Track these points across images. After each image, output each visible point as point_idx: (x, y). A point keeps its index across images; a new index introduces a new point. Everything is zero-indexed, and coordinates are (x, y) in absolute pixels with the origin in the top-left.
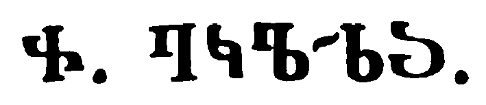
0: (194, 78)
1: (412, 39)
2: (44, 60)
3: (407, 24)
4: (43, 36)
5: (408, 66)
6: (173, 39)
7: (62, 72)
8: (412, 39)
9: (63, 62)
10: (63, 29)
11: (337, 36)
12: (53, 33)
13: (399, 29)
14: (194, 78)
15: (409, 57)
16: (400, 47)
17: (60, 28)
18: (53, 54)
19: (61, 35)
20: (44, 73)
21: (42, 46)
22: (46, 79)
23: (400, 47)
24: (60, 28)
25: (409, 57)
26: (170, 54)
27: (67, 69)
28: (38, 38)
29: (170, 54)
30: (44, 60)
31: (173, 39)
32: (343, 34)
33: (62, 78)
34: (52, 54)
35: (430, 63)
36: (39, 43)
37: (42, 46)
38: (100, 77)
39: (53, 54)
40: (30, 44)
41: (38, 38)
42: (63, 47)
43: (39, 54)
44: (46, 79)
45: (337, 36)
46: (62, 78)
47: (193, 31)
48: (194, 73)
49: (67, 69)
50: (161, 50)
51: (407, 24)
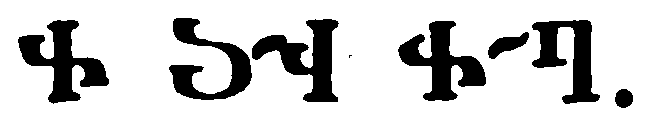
0: (335, 99)
1: (204, 43)
2: (50, 70)
3: (197, 22)
4: (49, 35)
5: (198, 82)
6: (566, 42)
7: (76, 87)
8: (204, 43)
9: (78, 73)
10: (78, 25)
11: (525, 36)
12: (63, 30)
13: (185, 30)
14: (335, 99)
15: (200, 69)
16: (187, 54)
17: (74, 24)
18: (63, 62)
19: (74, 34)
20: (50, 90)
21: (47, 50)
22: (53, 99)
23: (187, 54)
24: (74, 24)
25: (200, 69)
26: (563, 62)
27: (84, 84)
28: (41, 38)
29: (563, 62)
30: (50, 70)
31: (566, 42)
32: (535, 37)
33: (76, 97)
34: (64, 63)
35: (230, 78)
36: (42, 46)
37: (47, 50)
38: (624, 99)
39: (63, 62)
40: (29, 48)
41: (41, 38)
42: (77, 52)
43: (43, 62)
44: (53, 99)
45: (525, 36)
46: (76, 97)
47: (453, 30)
48: (335, 91)
49: (84, 84)
50: (548, 58)
51: (197, 22)
